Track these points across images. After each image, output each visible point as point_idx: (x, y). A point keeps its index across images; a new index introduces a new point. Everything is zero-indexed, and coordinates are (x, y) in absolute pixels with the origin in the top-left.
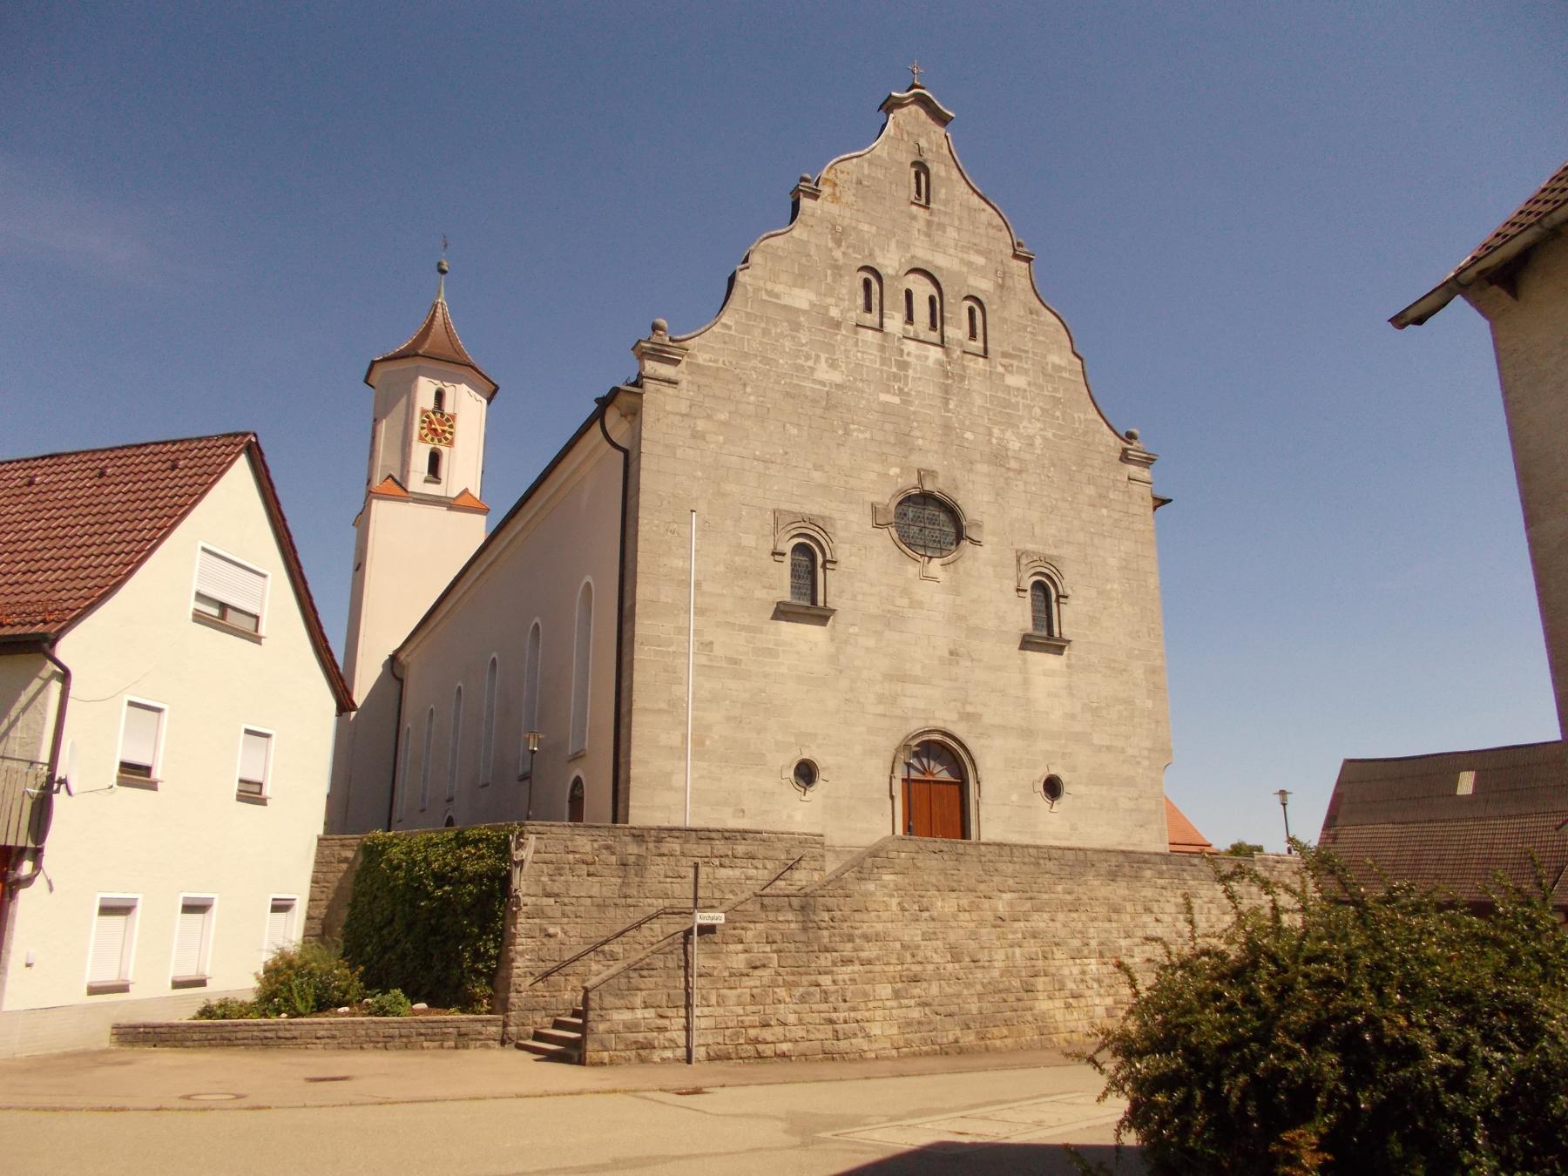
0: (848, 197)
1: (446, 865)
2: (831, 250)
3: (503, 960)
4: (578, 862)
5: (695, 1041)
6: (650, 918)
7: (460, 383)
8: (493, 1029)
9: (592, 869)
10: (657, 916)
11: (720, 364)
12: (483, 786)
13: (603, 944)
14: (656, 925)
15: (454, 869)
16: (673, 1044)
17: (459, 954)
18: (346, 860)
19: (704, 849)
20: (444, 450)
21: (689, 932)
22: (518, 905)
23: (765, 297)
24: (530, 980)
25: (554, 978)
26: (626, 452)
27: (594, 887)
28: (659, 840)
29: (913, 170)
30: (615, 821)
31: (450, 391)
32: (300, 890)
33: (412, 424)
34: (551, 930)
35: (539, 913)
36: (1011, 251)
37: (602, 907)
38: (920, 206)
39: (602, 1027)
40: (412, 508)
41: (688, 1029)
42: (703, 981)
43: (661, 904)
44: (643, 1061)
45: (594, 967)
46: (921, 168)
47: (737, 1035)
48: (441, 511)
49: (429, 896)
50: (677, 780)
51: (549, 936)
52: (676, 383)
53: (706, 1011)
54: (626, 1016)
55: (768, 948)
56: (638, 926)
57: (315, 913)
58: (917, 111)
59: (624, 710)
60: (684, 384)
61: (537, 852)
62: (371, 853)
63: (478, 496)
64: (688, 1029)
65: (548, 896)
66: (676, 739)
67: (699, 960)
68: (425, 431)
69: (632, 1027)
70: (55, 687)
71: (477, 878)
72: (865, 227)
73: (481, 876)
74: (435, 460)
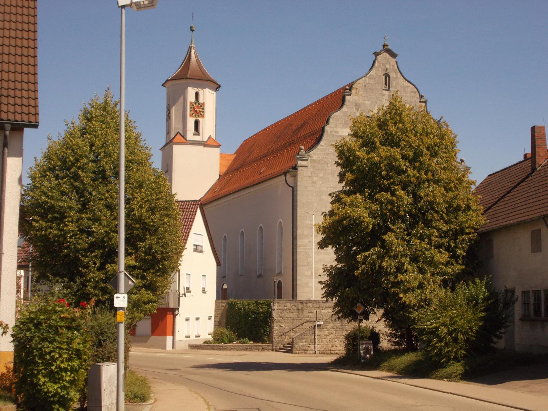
0: (361, 92)
1: (254, 309)
2: (355, 113)
3: (271, 332)
4: (287, 309)
5: (317, 349)
6: (305, 323)
7: (205, 88)
8: (270, 347)
9: (291, 311)
10: (306, 322)
11: (320, 159)
12: (240, 276)
13: (294, 328)
14: (306, 324)
15: (257, 311)
16: (312, 350)
17: (260, 331)
18: (223, 306)
19: (318, 305)
20: (200, 119)
21: (315, 326)
22: (274, 319)
23: (334, 133)
24: (277, 337)
25: (283, 336)
26: (293, 187)
27: (291, 315)
28: (307, 303)
29: (384, 77)
30: (293, 298)
31: (201, 92)
32: (213, 315)
33: (186, 109)
34: (282, 325)
35: (279, 321)
36: (419, 100)
37: (293, 320)
38: (386, 90)
39: (296, 346)
40: (189, 147)
41: (315, 347)
42: (318, 337)
43: (307, 319)
44: (305, 353)
45: (292, 334)
46: (387, 76)
47: (326, 349)
48: (201, 148)
49: (250, 317)
50: (310, 284)
51: (281, 327)
52: (307, 167)
53: (319, 343)
54: (302, 344)
55: (333, 330)
56: (302, 324)
57: (216, 320)
58: (386, 55)
59: (295, 265)
60: (309, 167)
61: (278, 307)
62: (231, 306)
63: (214, 139)
64: (315, 347)
65: (280, 317)
66: (309, 273)
67: (317, 332)
68: (192, 112)
69: (303, 346)
70: (177, 273)
71: (263, 313)
72: (366, 102)
73: (264, 313)
74: (197, 123)
